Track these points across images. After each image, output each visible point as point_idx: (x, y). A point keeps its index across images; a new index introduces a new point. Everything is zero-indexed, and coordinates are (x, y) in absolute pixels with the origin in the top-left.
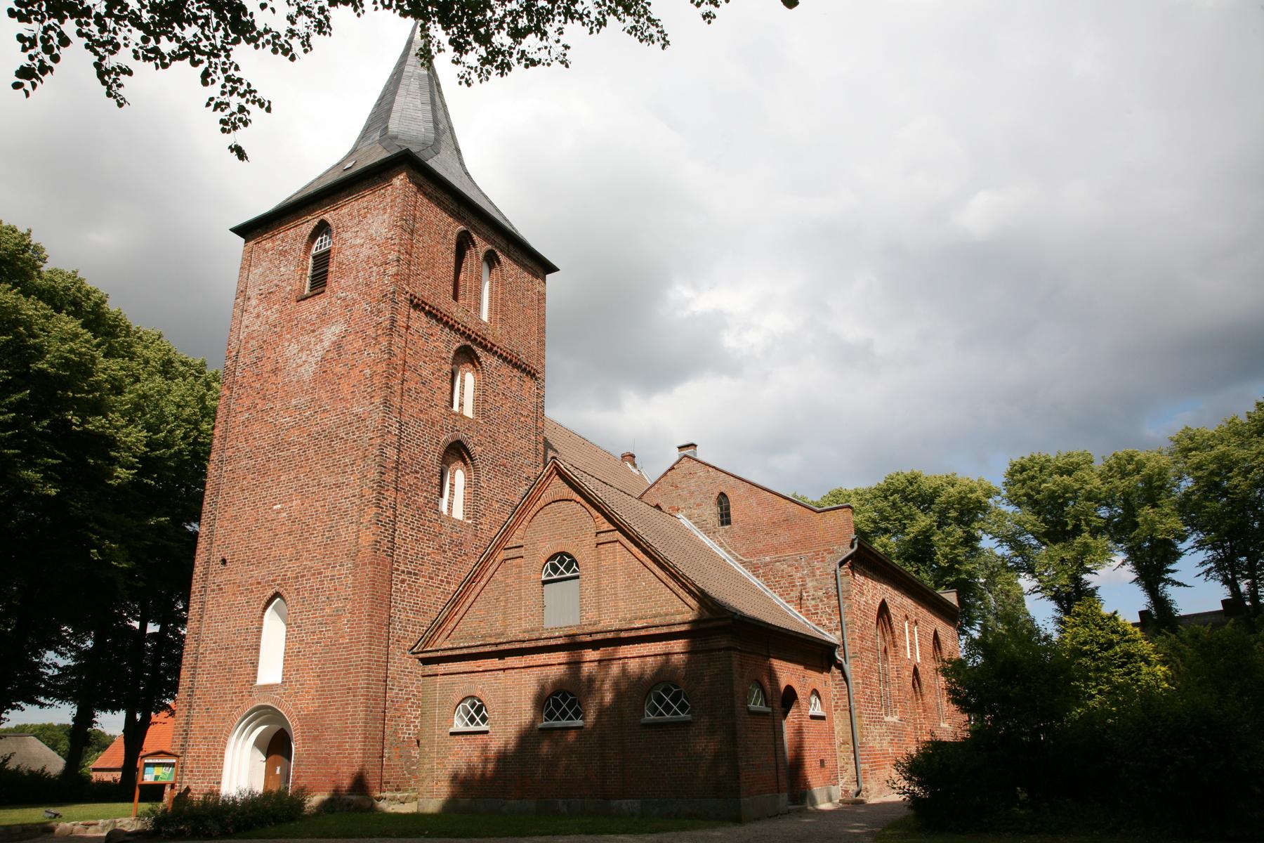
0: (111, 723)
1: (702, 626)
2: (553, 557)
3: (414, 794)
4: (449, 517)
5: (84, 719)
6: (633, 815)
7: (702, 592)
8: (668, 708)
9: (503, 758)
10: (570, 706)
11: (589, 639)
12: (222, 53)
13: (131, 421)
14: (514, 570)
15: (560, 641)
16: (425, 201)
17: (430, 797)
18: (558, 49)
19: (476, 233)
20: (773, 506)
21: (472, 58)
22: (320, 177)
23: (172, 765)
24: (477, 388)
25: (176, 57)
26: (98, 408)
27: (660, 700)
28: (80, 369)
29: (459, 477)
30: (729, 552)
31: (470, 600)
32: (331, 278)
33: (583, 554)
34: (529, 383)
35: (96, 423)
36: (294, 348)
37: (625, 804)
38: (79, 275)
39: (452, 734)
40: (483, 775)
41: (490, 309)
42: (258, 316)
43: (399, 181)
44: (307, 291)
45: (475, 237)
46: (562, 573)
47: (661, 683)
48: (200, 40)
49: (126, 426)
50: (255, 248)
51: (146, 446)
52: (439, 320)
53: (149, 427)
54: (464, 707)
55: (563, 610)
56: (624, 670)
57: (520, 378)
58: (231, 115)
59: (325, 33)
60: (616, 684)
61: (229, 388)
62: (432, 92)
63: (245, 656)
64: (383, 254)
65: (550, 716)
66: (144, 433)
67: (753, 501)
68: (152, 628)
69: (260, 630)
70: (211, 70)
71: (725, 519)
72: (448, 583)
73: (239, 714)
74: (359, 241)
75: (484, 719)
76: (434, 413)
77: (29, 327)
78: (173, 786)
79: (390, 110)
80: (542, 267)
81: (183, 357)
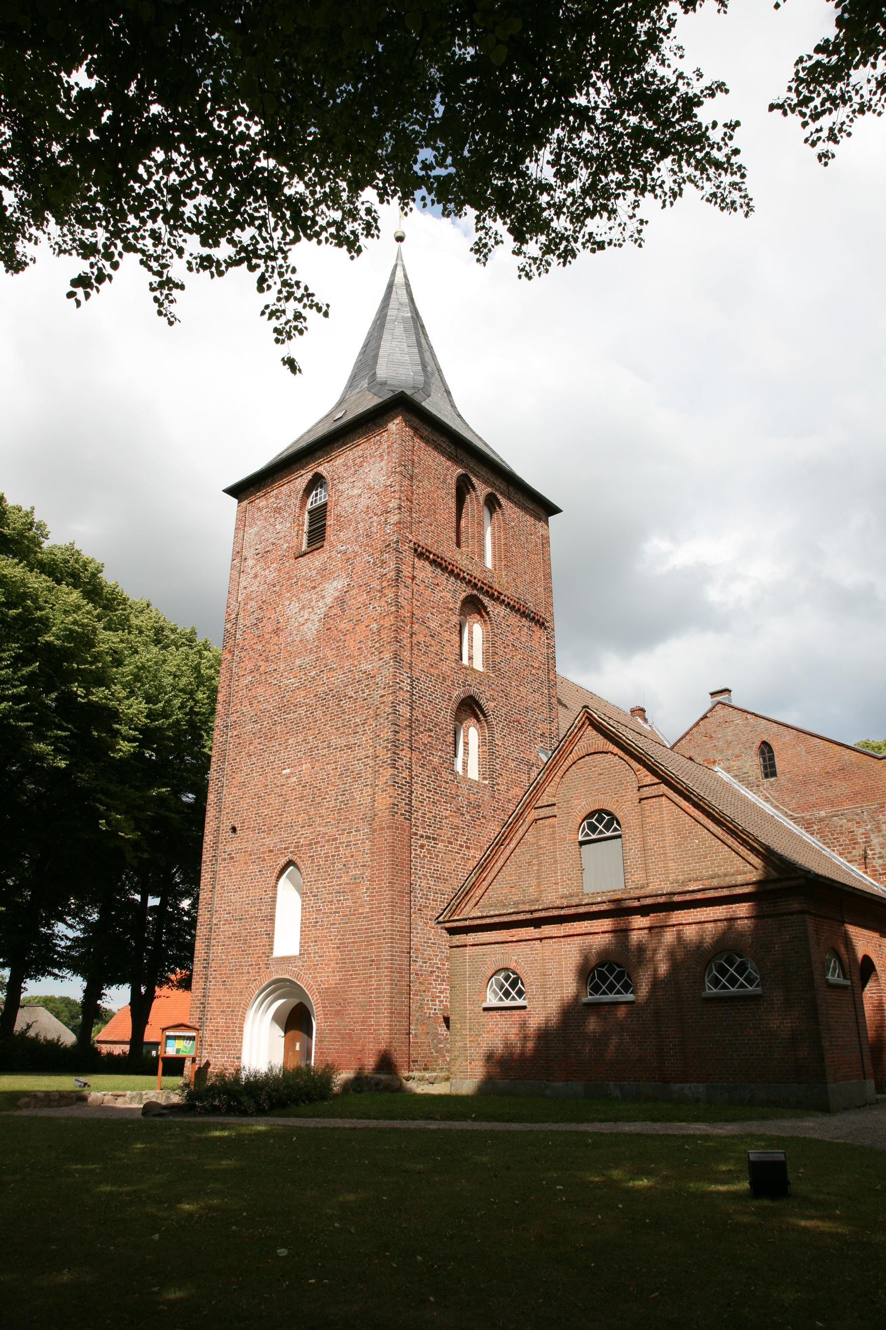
0: (117, 998)
1: (771, 886)
2: (590, 815)
3: (443, 1074)
4: (465, 778)
5: (93, 993)
6: (697, 1100)
7: (767, 848)
8: (733, 981)
9: (544, 1035)
10: (618, 978)
11: (636, 904)
12: (280, 255)
13: (132, 693)
14: (548, 831)
15: (603, 907)
16: (423, 445)
17: (465, 1079)
18: (633, 225)
19: (475, 475)
20: (825, 754)
21: (533, 248)
22: (309, 431)
23: (192, 1038)
24: (486, 640)
25: (233, 263)
26: (101, 680)
27: (723, 971)
28: (82, 640)
29: (472, 734)
30: (776, 807)
31: (499, 864)
32: (329, 532)
33: (625, 809)
34: (539, 632)
35: (99, 694)
36: (295, 606)
37: (690, 1089)
38: (77, 547)
39: (485, 1009)
40: (522, 1054)
41: (494, 556)
42: (256, 576)
43: (396, 426)
44: (304, 548)
45: (474, 480)
46: (601, 832)
47: (723, 951)
48: (257, 242)
49: (127, 698)
50: (249, 507)
51: (147, 717)
52: (445, 569)
53: (149, 699)
54: (497, 980)
55: (604, 873)
56: (679, 937)
57: (529, 628)
58: (286, 323)
59: (373, 236)
60: (671, 954)
61: (230, 652)
62: (417, 334)
63: (260, 927)
64: (383, 503)
65: (596, 989)
66: (143, 705)
67: (801, 749)
68: (154, 901)
69: (274, 899)
70: (267, 275)
71: (770, 770)
72: (468, 847)
73: (257, 987)
74: (356, 492)
75: (520, 993)
76: (445, 667)
77: (35, 600)
78: (194, 1060)
79: (376, 357)
80: (544, 508)
81: (172, 624)
